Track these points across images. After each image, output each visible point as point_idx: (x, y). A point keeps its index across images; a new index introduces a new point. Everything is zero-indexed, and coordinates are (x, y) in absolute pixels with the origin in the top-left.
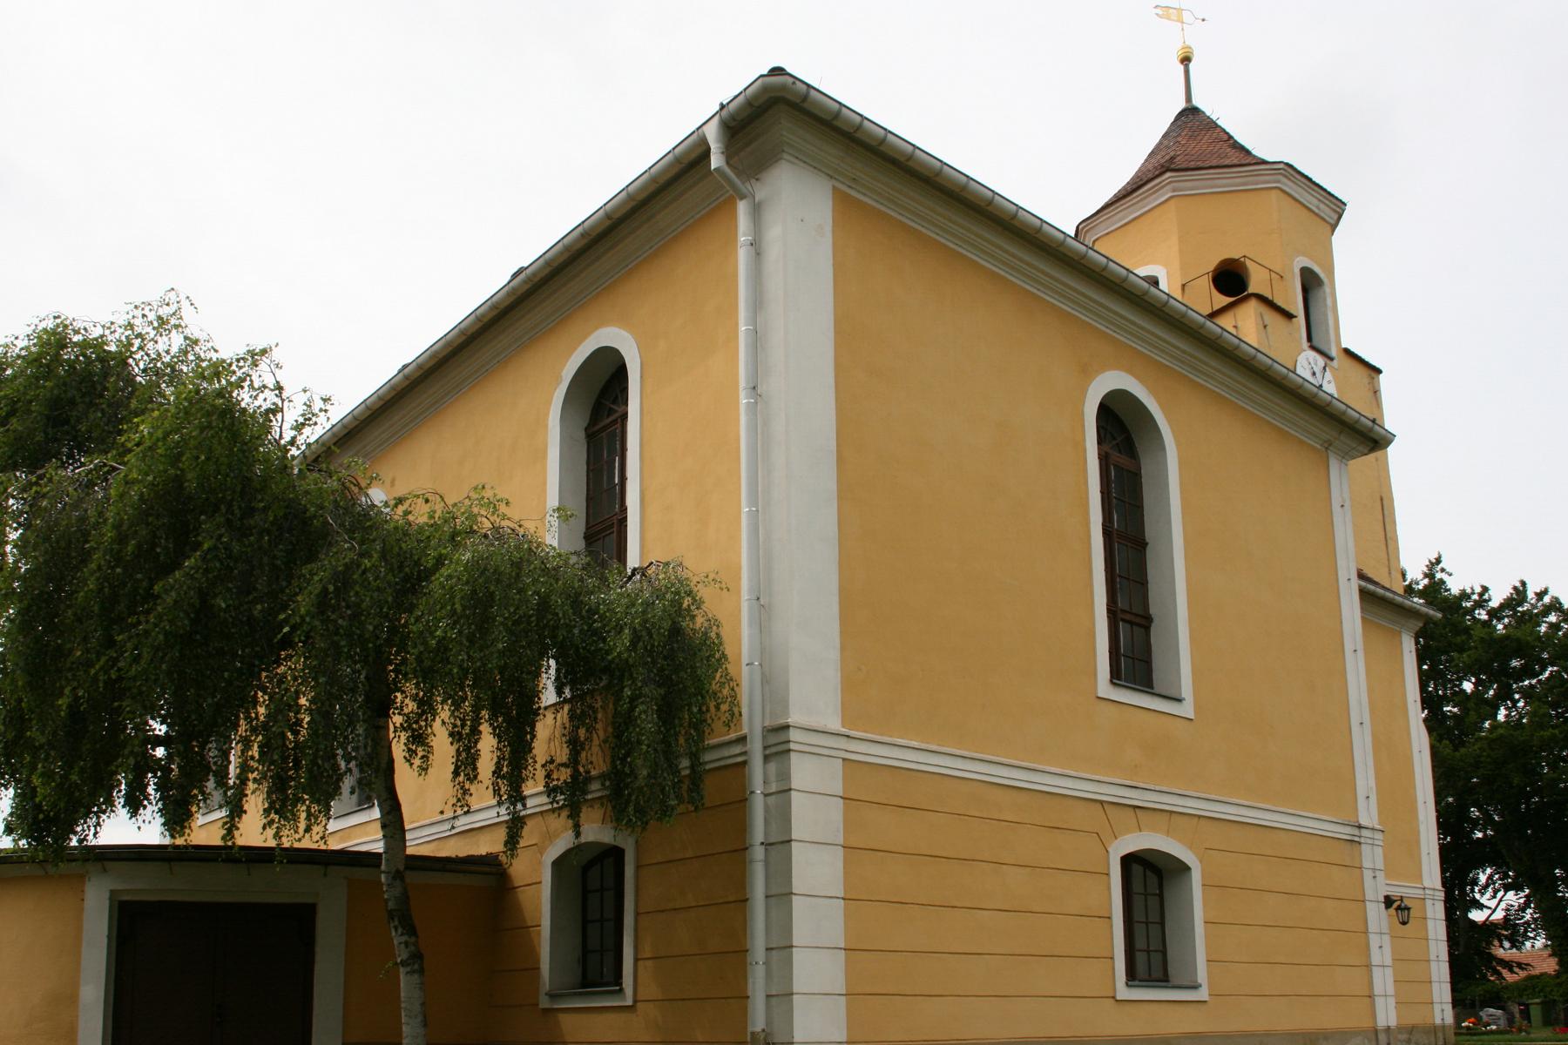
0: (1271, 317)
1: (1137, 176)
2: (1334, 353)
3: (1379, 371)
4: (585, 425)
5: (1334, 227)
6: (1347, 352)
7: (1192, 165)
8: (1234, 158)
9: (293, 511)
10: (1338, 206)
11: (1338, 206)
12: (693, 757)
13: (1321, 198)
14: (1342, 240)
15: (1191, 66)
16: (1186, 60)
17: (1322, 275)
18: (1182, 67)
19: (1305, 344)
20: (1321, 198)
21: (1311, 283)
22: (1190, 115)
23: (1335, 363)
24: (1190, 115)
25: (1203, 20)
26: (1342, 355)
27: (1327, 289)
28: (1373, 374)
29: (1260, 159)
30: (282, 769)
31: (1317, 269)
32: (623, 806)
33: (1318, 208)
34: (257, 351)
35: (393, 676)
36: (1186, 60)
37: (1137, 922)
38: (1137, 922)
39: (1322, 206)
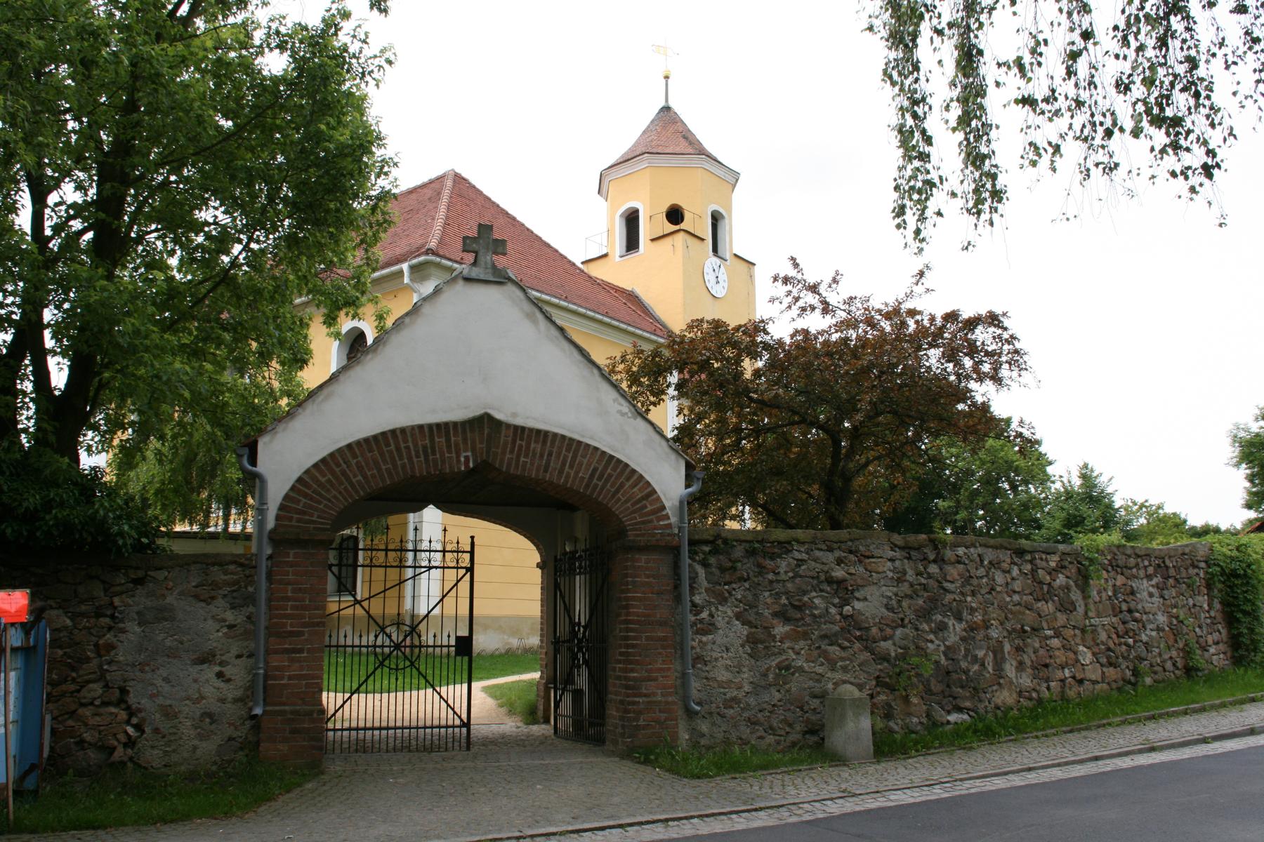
0: (690, 240)
3: (754, 264)
4: (347, 352)
5: (734, 186)
6: (735, 255)
7: (654, 151)
8: (682, 146)
9: (112, 288)
10: (736, 176)
11: (736, 176)
12: (817, 677)
14: (738, 195)
16: (667, 77)
17: (724, 213)
18: (664, 81)
19: (711, 253)
21: (716, 218)
22: (666, 109)
23: (728, 263)
24: (666, 109)
26: (733, 257)
27: (727, 221)
30: (1230, 587)
31: (721, 210)
36: (667, 77)
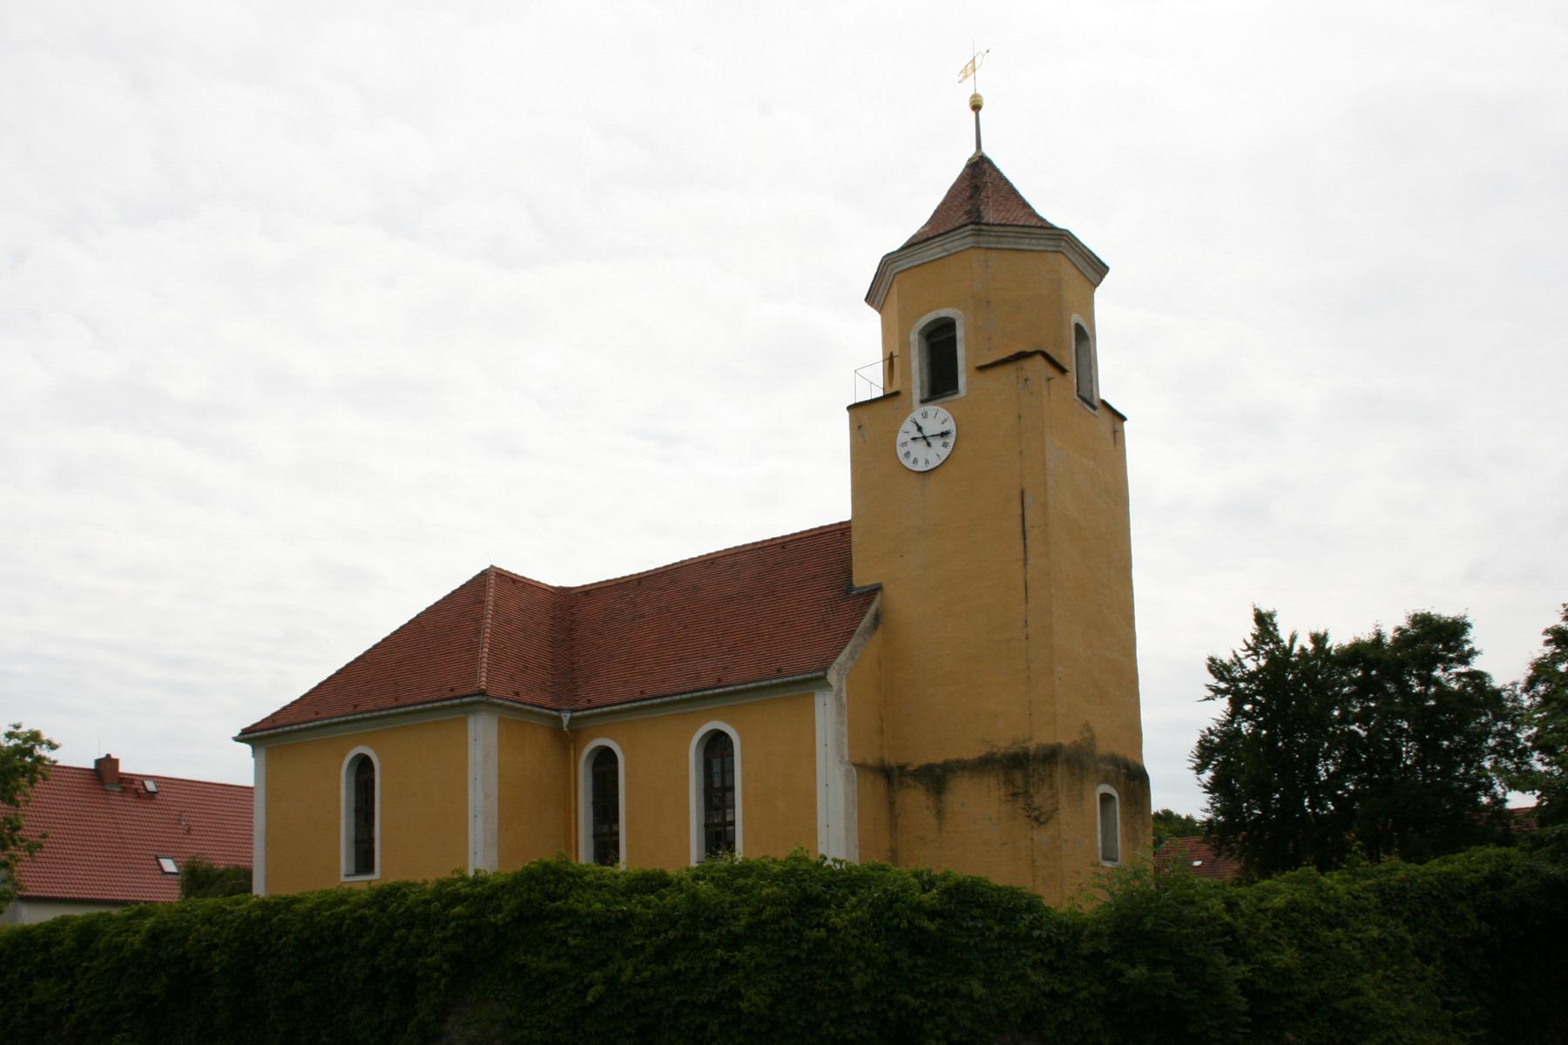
1: (908, 242)
2: (1096, 403)
3: (1123, 419)
5: (1096, 285)
10: (1101, 269)
11: (1101, 269)
13: (942, 243)
15: (981, 113)
16: (976, 107)
20: (942, 243)
25: (988, 51)
28: (1117, 420)
29: (1048, 223)
32: (1344, 993)
33: (945, 250)
34: (910, 768)
35: (1067, 1018)
36: (976, 107)
37: (718, 836)
38: (718, 836)
39: (947, 246)
